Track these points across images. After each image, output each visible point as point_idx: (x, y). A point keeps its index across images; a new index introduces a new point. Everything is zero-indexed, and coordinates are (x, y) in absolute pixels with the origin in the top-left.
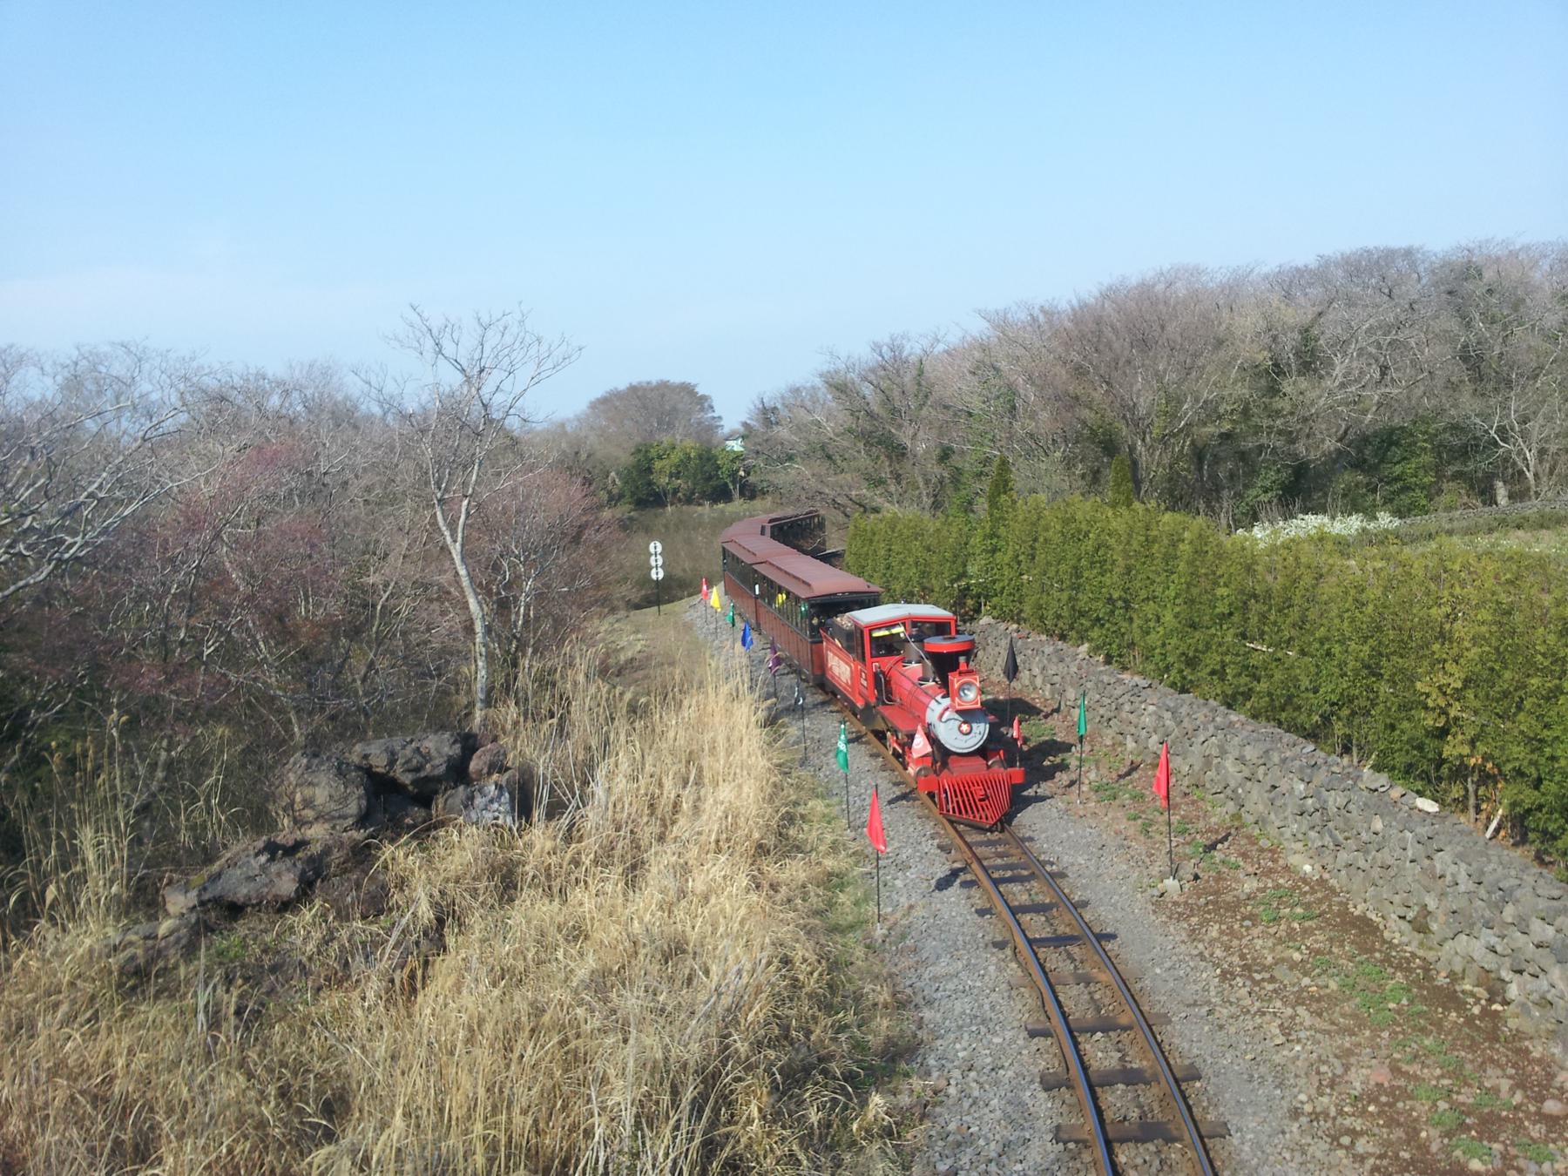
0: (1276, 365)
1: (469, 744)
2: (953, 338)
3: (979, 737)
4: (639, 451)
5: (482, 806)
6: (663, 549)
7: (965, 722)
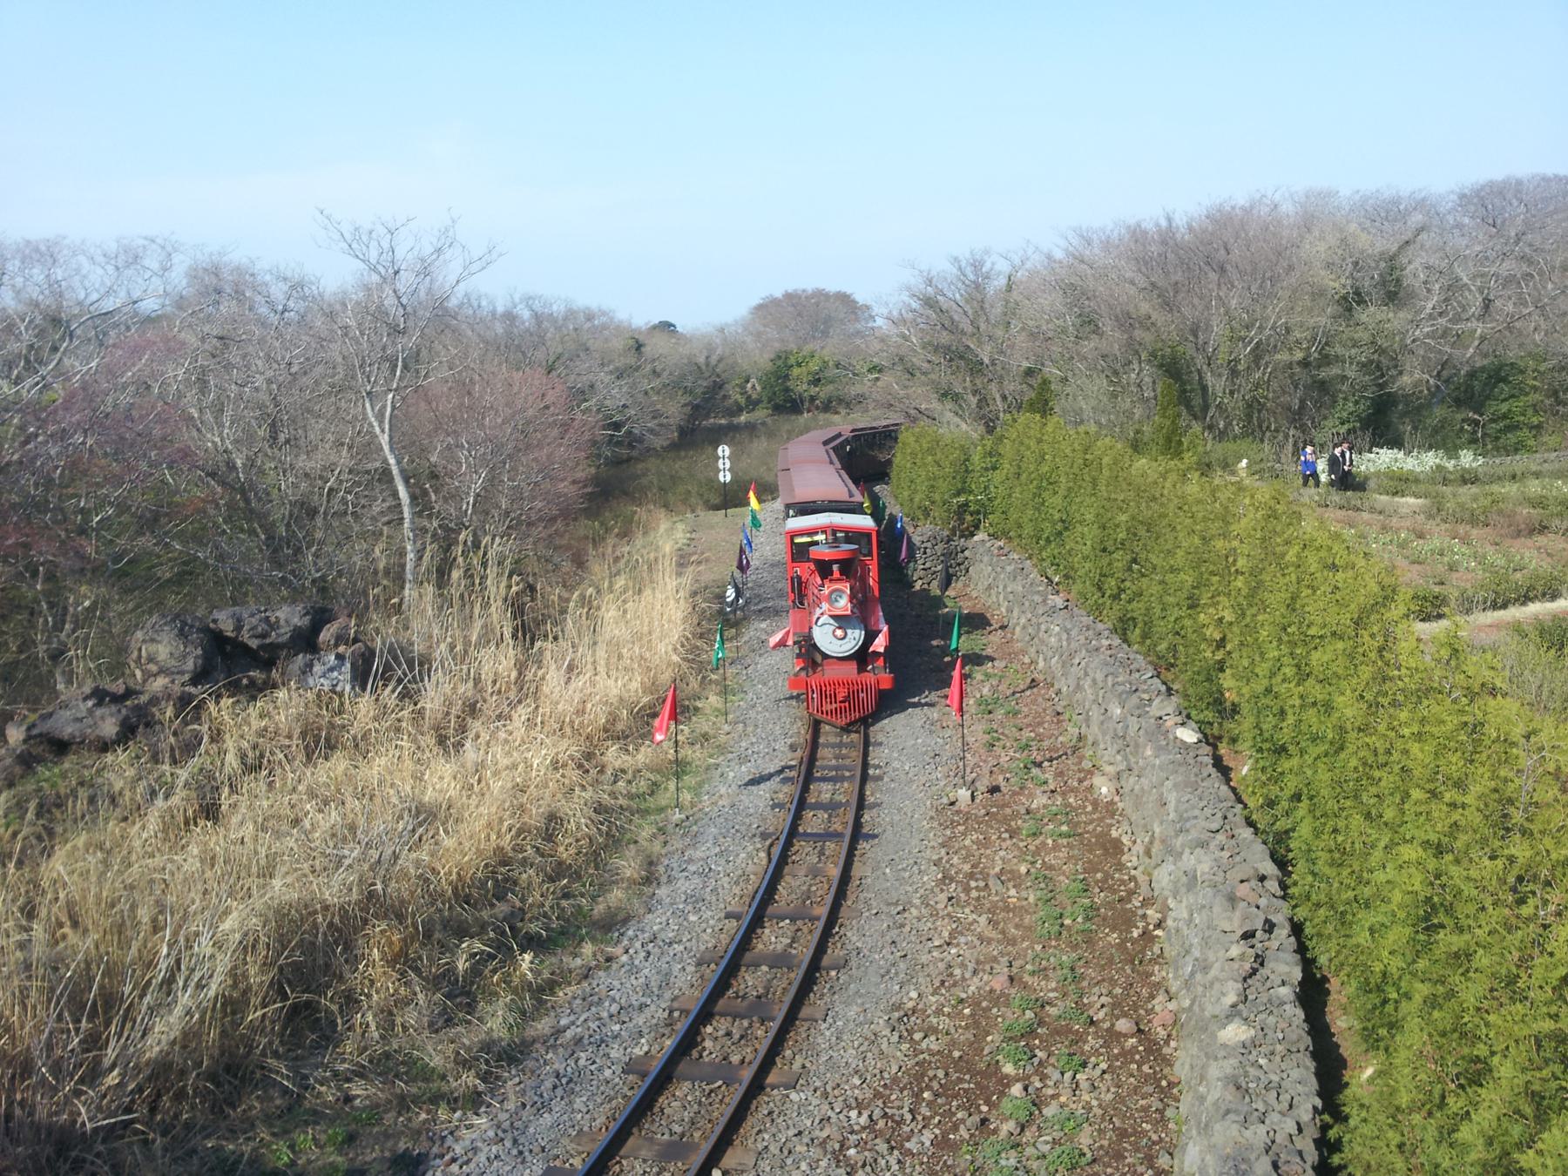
0: (1357, 293)
1: (321, 617)
2: (1036, 261)
3: (854, 643)
4: (780, 357)
5: (320, 673)
6: (731, 453)
7: (839, 628)
